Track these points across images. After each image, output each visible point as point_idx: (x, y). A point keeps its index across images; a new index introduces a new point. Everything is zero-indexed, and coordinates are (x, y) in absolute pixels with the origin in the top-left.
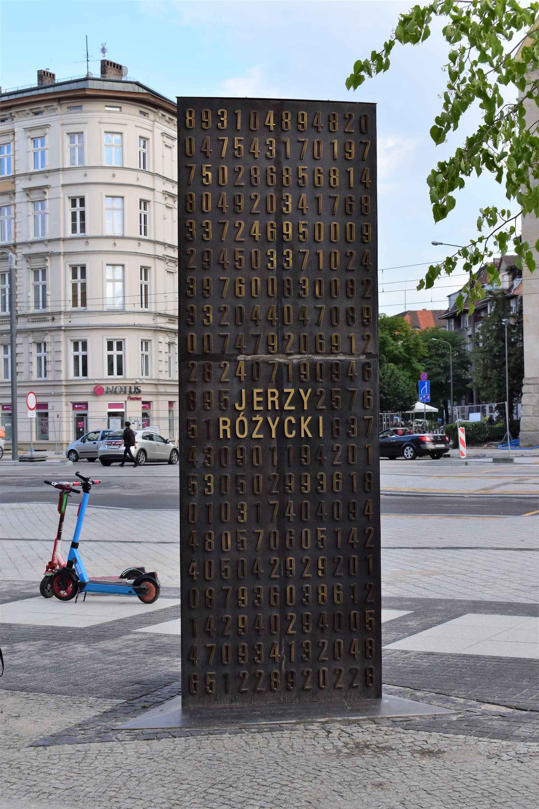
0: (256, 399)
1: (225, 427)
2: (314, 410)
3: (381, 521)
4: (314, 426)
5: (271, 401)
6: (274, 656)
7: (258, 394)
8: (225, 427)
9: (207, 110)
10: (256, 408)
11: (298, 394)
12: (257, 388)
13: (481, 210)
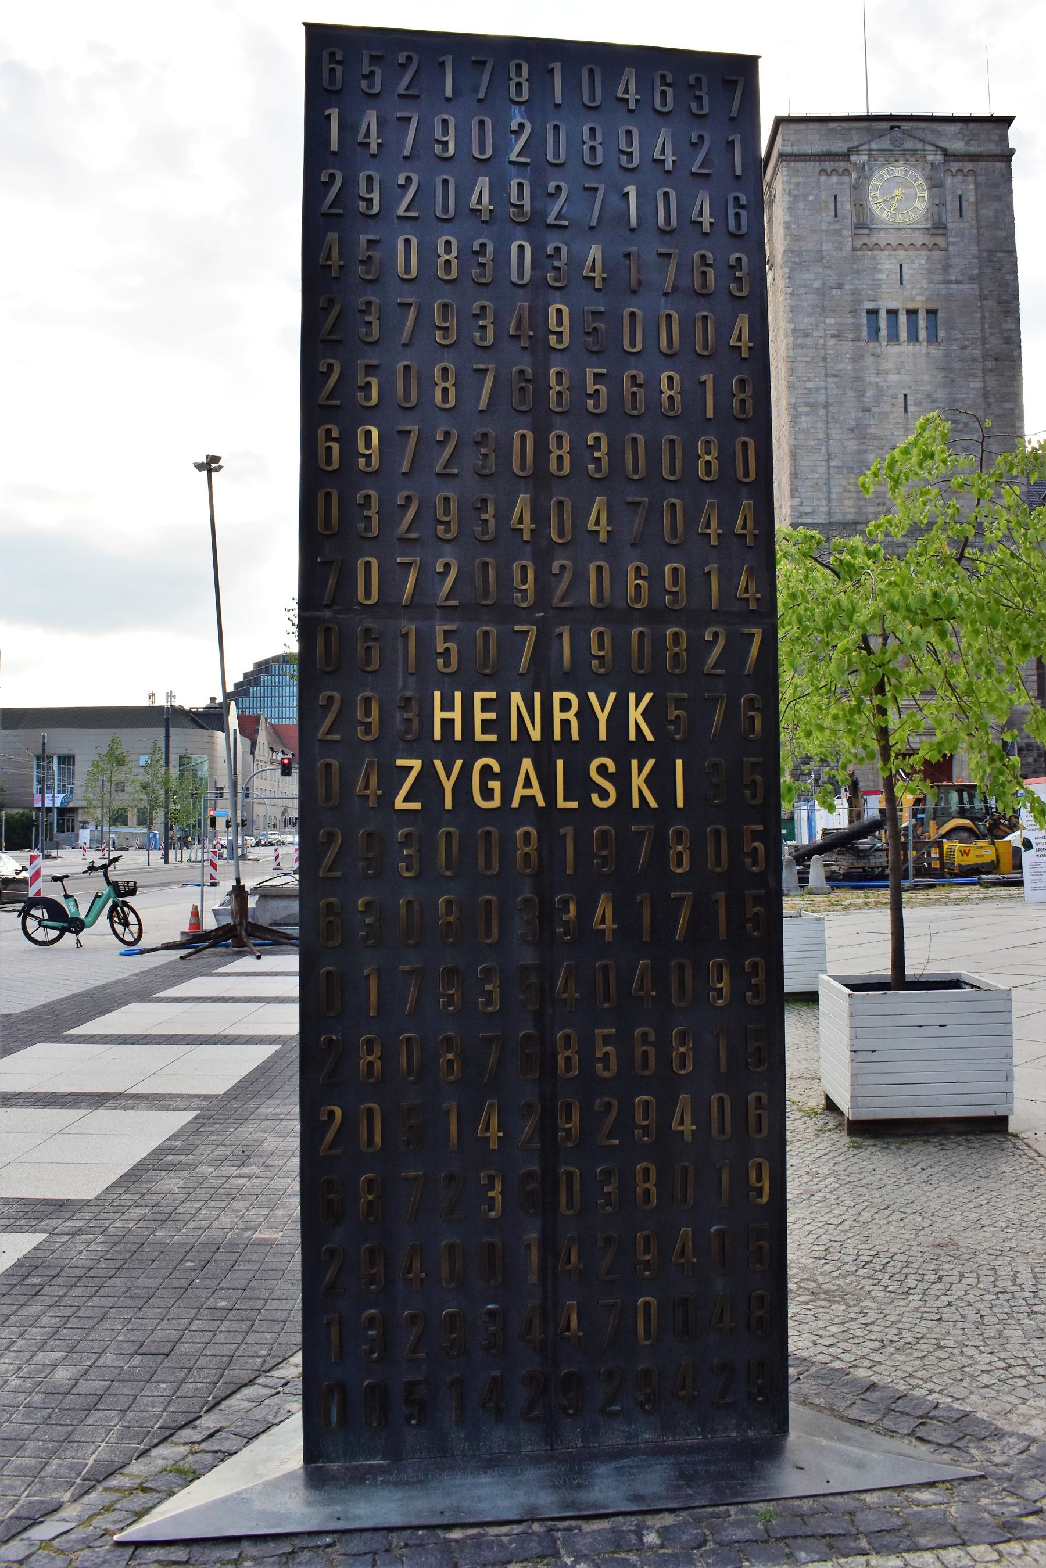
0: (479, 716)
1: (565, 716)
2: (662, 750)
3: (786, 942)
4: (660, 781)
5: (562, 720)
6: (681, 1128)
7: (486, 705)
8: (565, 716)
9: (446, 117)
10: (479, 736)
11: (428, 774)
12: (479, 690)
13: (207, 456)
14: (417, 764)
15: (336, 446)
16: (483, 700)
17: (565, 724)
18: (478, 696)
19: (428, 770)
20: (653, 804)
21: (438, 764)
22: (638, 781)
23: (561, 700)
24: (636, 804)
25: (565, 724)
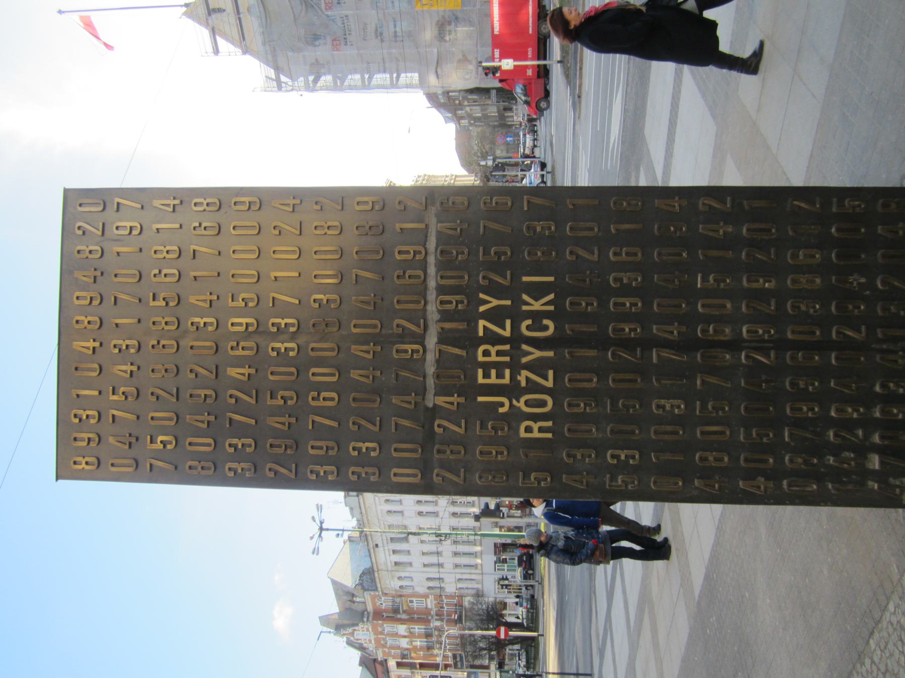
0: (493, 380)
1: (493, 353)
5: (497, 355)
7: (486, 375)
12: (476, 379)
14: (482, 323)
15: (323, 394)
16: (484, 377)
17: (498, 353)
18: (481, 380)
19: (486, 316)
20: (552, 296)
21: (482, 309)
22: (537, 306)
23: (526, 431)
24: (552, 308)
25: (498, 353)
